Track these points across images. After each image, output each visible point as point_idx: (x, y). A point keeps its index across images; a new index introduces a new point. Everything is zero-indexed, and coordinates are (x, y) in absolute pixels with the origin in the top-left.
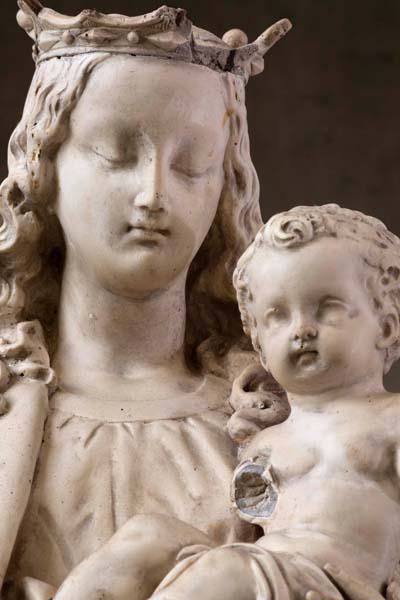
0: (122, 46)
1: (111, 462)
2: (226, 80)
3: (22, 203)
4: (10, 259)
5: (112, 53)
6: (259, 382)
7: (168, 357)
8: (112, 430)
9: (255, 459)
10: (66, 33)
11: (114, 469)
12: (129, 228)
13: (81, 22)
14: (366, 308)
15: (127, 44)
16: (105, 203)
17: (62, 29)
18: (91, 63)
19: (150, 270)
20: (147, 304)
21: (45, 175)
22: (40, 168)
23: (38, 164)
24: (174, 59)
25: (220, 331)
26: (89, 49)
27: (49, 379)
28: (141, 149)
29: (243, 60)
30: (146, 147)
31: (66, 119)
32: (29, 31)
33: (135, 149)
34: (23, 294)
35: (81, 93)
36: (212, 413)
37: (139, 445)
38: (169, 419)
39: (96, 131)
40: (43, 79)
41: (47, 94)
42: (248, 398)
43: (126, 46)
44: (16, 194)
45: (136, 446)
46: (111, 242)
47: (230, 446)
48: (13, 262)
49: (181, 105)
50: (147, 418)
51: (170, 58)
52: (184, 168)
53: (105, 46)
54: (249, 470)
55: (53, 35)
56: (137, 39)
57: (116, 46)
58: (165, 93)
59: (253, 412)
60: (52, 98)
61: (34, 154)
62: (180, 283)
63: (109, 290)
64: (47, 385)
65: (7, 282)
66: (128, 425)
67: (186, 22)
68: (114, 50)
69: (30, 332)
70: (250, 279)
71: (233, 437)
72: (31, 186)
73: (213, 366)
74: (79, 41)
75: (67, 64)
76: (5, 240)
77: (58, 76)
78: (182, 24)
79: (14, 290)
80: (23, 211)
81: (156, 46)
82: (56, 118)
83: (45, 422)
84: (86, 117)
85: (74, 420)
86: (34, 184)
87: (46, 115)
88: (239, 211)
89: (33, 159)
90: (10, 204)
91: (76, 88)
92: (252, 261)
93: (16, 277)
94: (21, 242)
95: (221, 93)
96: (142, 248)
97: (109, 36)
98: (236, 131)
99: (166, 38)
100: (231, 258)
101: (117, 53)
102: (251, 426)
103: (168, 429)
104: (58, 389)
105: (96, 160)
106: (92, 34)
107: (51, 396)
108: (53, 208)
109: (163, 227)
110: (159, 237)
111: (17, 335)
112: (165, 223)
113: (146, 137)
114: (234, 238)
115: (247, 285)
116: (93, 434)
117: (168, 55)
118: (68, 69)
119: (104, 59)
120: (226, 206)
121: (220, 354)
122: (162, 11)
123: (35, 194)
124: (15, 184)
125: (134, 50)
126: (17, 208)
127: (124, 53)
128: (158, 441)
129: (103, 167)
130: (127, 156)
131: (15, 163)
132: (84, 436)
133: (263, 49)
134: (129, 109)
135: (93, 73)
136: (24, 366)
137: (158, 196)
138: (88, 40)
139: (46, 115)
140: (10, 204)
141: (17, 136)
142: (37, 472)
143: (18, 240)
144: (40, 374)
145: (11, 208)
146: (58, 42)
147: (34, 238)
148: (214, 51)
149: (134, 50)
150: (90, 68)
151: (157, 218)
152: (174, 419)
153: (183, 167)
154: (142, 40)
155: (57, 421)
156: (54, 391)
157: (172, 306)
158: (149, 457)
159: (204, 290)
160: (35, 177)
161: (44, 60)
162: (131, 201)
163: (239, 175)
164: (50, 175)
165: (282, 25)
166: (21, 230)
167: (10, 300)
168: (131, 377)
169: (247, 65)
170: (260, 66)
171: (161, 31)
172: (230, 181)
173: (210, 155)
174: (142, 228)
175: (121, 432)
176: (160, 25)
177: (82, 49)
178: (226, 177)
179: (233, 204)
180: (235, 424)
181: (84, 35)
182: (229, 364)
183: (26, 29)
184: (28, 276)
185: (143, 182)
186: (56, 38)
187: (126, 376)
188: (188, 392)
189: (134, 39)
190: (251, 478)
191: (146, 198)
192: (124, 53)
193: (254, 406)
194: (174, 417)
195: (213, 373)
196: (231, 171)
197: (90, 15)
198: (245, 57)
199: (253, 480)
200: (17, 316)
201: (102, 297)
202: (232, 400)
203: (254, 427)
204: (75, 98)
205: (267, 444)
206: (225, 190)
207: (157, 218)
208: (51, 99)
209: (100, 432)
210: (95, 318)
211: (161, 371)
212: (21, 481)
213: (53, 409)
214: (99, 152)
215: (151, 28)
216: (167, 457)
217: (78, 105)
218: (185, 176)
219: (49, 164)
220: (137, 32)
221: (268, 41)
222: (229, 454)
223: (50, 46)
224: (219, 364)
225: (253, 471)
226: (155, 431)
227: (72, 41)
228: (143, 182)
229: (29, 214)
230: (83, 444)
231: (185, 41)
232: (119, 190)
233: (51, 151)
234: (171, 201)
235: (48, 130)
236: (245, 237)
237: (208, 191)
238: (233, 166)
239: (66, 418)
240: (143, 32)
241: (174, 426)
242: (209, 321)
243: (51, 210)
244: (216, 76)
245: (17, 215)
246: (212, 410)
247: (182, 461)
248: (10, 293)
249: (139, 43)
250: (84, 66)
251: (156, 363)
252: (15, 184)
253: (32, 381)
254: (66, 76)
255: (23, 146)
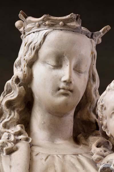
0: (57, 27)
1: (54, 166)
2: (91, 41)
3: (20, 83)
4: (15, 103)
5: (54, 29)
6: (102, 145)
7: (69, 138)
8: (53, 157)
9: (107, 162)
10: (37, 23)
11: (56, 168)
12: (59, 89)
13: (43, 19)
14: (105, 161)
15: (59, 26)
16: (51, 80)
17: (36, 22)
18: (46, 33)
19: (66, 104)
20: (62, 118)
21: (28, 73)
22: (27, 69)
23: (27, 69)
24: (75, 32)
25: (84, 132)
26: (45, 28)
27: (30, 141)
28: (64, 62)
29: (96, 36)
30: (66, 61)
31: (37, 52)
32: (20, 29)
33: (61, 62)
34: (18, 115)
35: (43, 43)
36: (86, 154)
37: (64, 162)
38: (72, 155)
39: (48, 56)
40: (28, 40)
41: (29, 46)
42: (99, 150)
43: (59, 27)
44: (17, 80)
45: (63, 162)
46: (53, 94)
47: (95, 163)
48: (16, 104)
49: (78, 47)
50: (65, 154)
51: (74, 31)
52: (78, 70)
53: (51, 27)
54: (105, 166)
55: (32, 25)
56: (63, 24)
57: (55, 27)
58: (73, 43)
59: (101, 153)
60: (32, 46)
61: (25, 65)
62: (72, 113)
63: (50, 113)
64: (29, 143)
65: (13, 111)
66: (59, 155)
67: (80, 20)
68: (55, 28)
69: (22, 127)
70: (105, 102)
71: (95, 161)
72: (24, 77)
73: (84, 141)
74: (42, 26)
75: (37, 34)
76: (13, 96)
77: (34, 38)
78: (78, 20)
79: (16, 113)
80: (20, 86)
81: (69, 27)
82: (33, 52)
83: (30, 154)
84: (44, 51)
85: (40, 154)
86: (25, 76)
87: (29, 52)
88: (94, 89)
89: (25, 67)
90: (15, 83)
91: (41, 41)
92: (106, 96)
93: (16, 109)
94: (19, 96)
95: (90, 45)
96: (63, 96)
97: (53, 23)
98: (94, 61)
99: (74, 24)
100: (89, 105)
101: (56, 29)
102: (101, 157)
103: (73, 157)
104: (33, 145)
105: (48, 66)
106: (47, 23)
107: (31, 147)
108: (30, 85)
109: (71, 89)
110: (69, 92)
111: (18, 128)
112: (72, 87)
113: (66, 58)
114: (91, 98)
115: (104, 104)
116: (47, 158)
117: (73, 30)
118: (38, 36)
119: (51, 31)
120: (89, 86)
121: (86, 137)
122: (72, 15)
123: (25, 80)
124: (17, 77)
125: (62, 28)
126: (18, 85)
127: (58, 29)
128: (70, 161)
129: (50, 68)
130: (59, 65)
131: (17, 70)
132: (44, 158)
133: (102, 34)
134: (60, 47)
135: (47, 36)
136: (20, 137)
137: (70, 77)
138: (45, 25)
139: (29, 52)
140: (15, 83)
141: (17, 61)
142: (29, 168)
143: (18, 95)
144: (27, 140)
145: (16, 85)
146: (34, 27)
147: (24, 95)
148: (87, 32)
149: (62, 28)
150: (46, 34)
151: (69, 85)
152: (74, 155)
153: (77, 69)
154: (65, 25)
155: (34, 154)
156: (31, 145)
157: (69, 119)
158: (67, 165)
159: (79, 118)
160: (25, 73)
161: (27, 35)
162: (60, 79)
163: (94, 76)
164: (30, 73)
165: (108, 27)
166: (19, 92)
167: (15, 117)
168: (57, 143)
169: (97, 38)
170: (100, 40)
171: (71, 22)
172: (91, 77)
173: (86, 66)
174: (64, 89)
175: (57, 157)
176: (71, 20)
177: (43, 29)
178: (89, 77)
179: (92, 86)
180: (95, 157)
181: (44, 24)
182: (89, 141)
183: (18, 28)
184: (20, 109)
185: (65, 73)
186: (33, 26)
187: (55, 143)
188: (77, 148)
189: (62, 24)
190: (106, 169)
191: (66, 78)
192: (58, 29)
193: (101, 151)
194: (74, 154)
195: (83, 144)
196: (91, 74)
197: (47, 16)
198: (96, 36)
199: (107, 170)
200: (16, 123)
201: (47, 115)
202: (92, 151)
203: (102, 158)
204: (40, 45)
205: (111, 158)
206: (89, 81)
207: (69, 85)
208: (32, 46)
209: (49, 157)
210: (44, 123)
211: (67, 142)
212: (25, 169)
213: (32, 151)
214: (49, 63)
215: (68, 20)
216: (73, 165)
217: (41, 48)
218: (78, 72)
219: (30, 70)
220: (63, 22)
221: (103, 32)
222: (94, 165)
223: (30, 29)
224: (86, 141)
225: (107, 166)
226: (68, 158)
227: (39, 26)
228: (65, 73)
229: (22, 87)
230: (44, 160)
231: (79, 26)
232: (56, 76)
233: (31, 64)
234: (73, 80)
235: (30, 57)
236: (95, 98)
237: (85, 79)
238: (92, 73)
239: (37, 153)
240: (65, 22)
241: (74, 156)
242: (81, 129)
243: (29, 86)
244: (89, 39)
245: (18, 87)
246: (86, 153)
247: (79, 166)
248: (15, 115)
249: (63, 26)
250: (44, 34)
251: (65, 139)
252: (17, 77)
253: (24, 141)
254: (37, 38)
255: (20, 64)
